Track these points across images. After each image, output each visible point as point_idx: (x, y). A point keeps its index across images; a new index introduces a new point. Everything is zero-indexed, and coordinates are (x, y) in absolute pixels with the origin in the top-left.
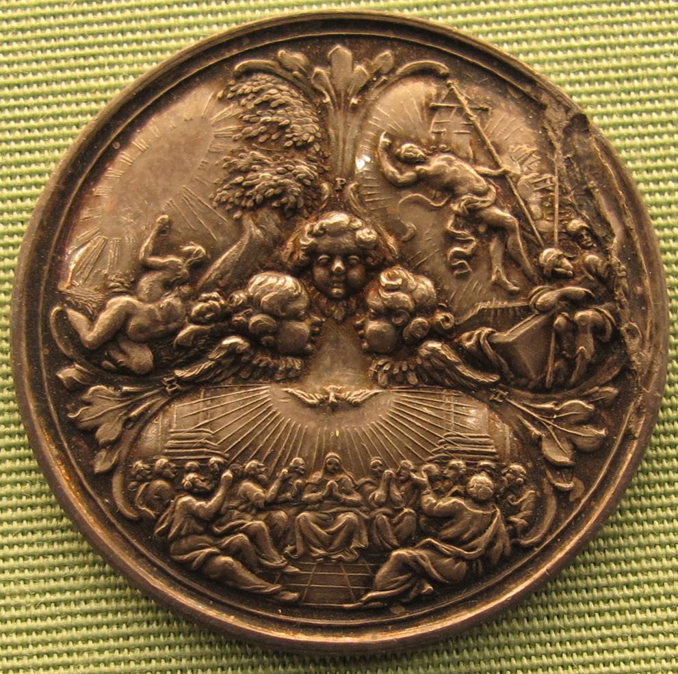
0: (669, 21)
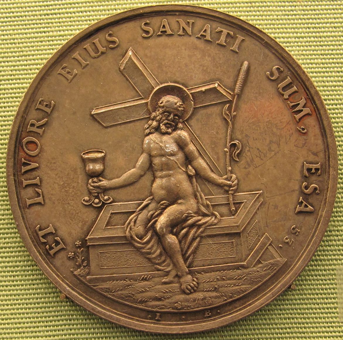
0: (339, 81)
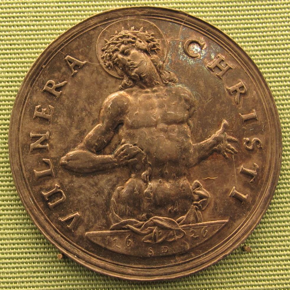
0: (286, 26)
